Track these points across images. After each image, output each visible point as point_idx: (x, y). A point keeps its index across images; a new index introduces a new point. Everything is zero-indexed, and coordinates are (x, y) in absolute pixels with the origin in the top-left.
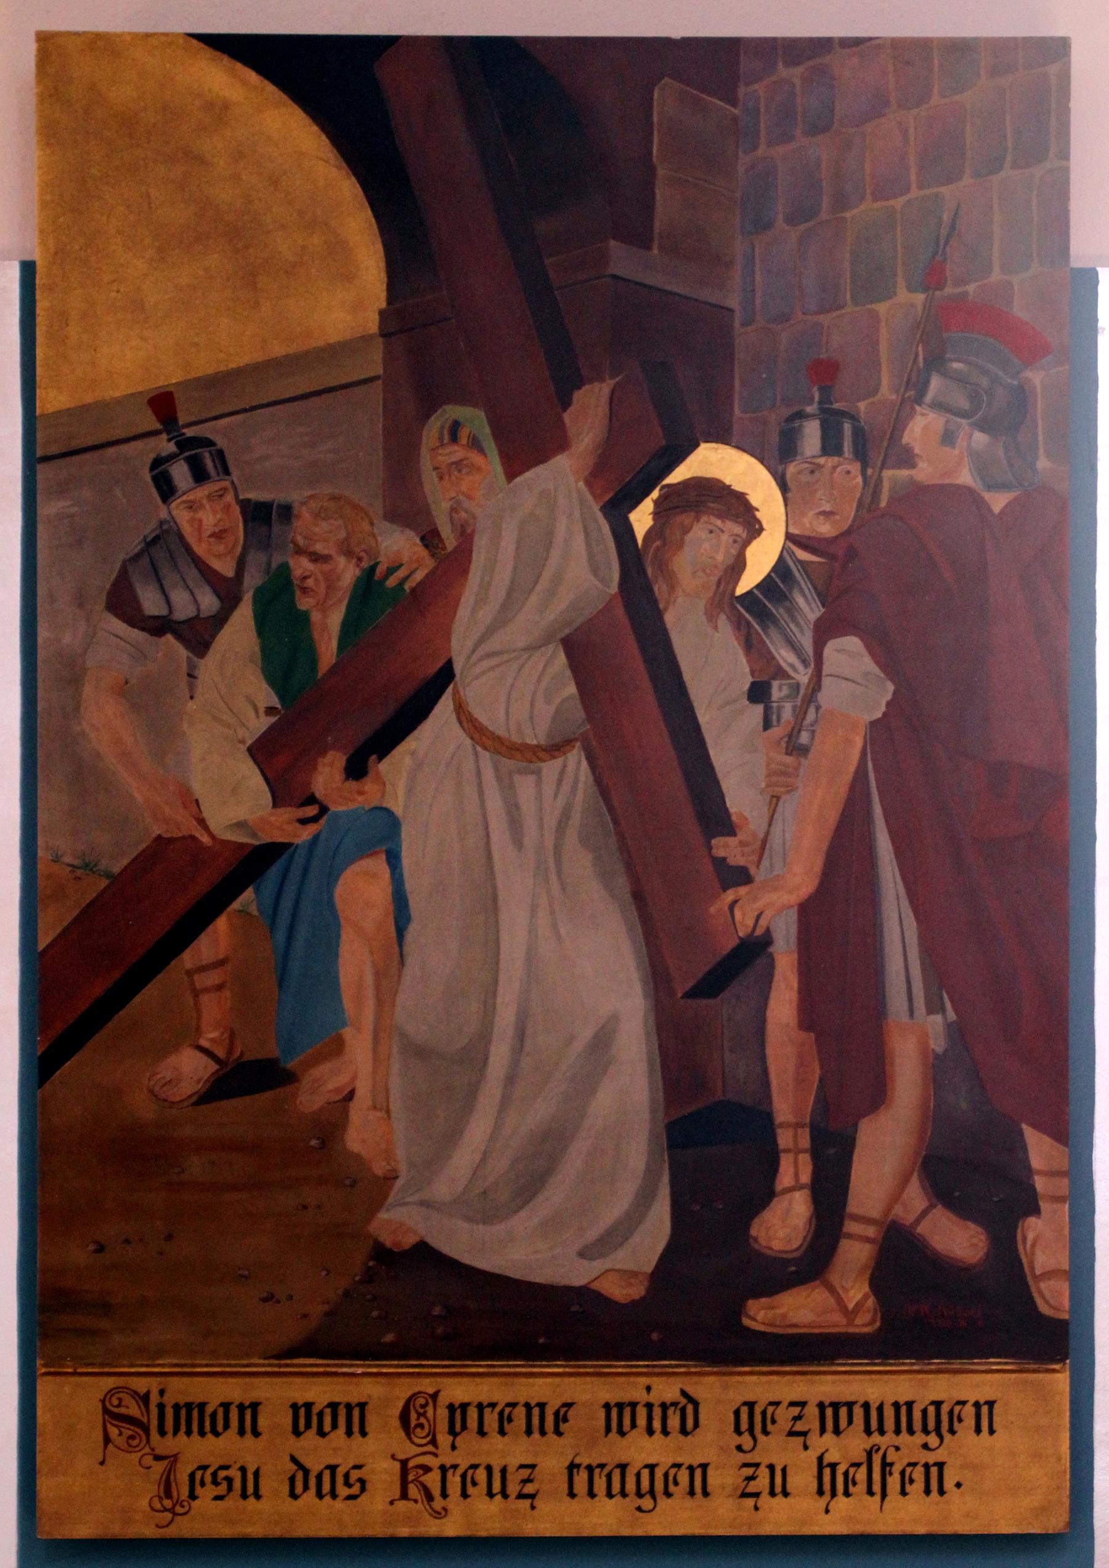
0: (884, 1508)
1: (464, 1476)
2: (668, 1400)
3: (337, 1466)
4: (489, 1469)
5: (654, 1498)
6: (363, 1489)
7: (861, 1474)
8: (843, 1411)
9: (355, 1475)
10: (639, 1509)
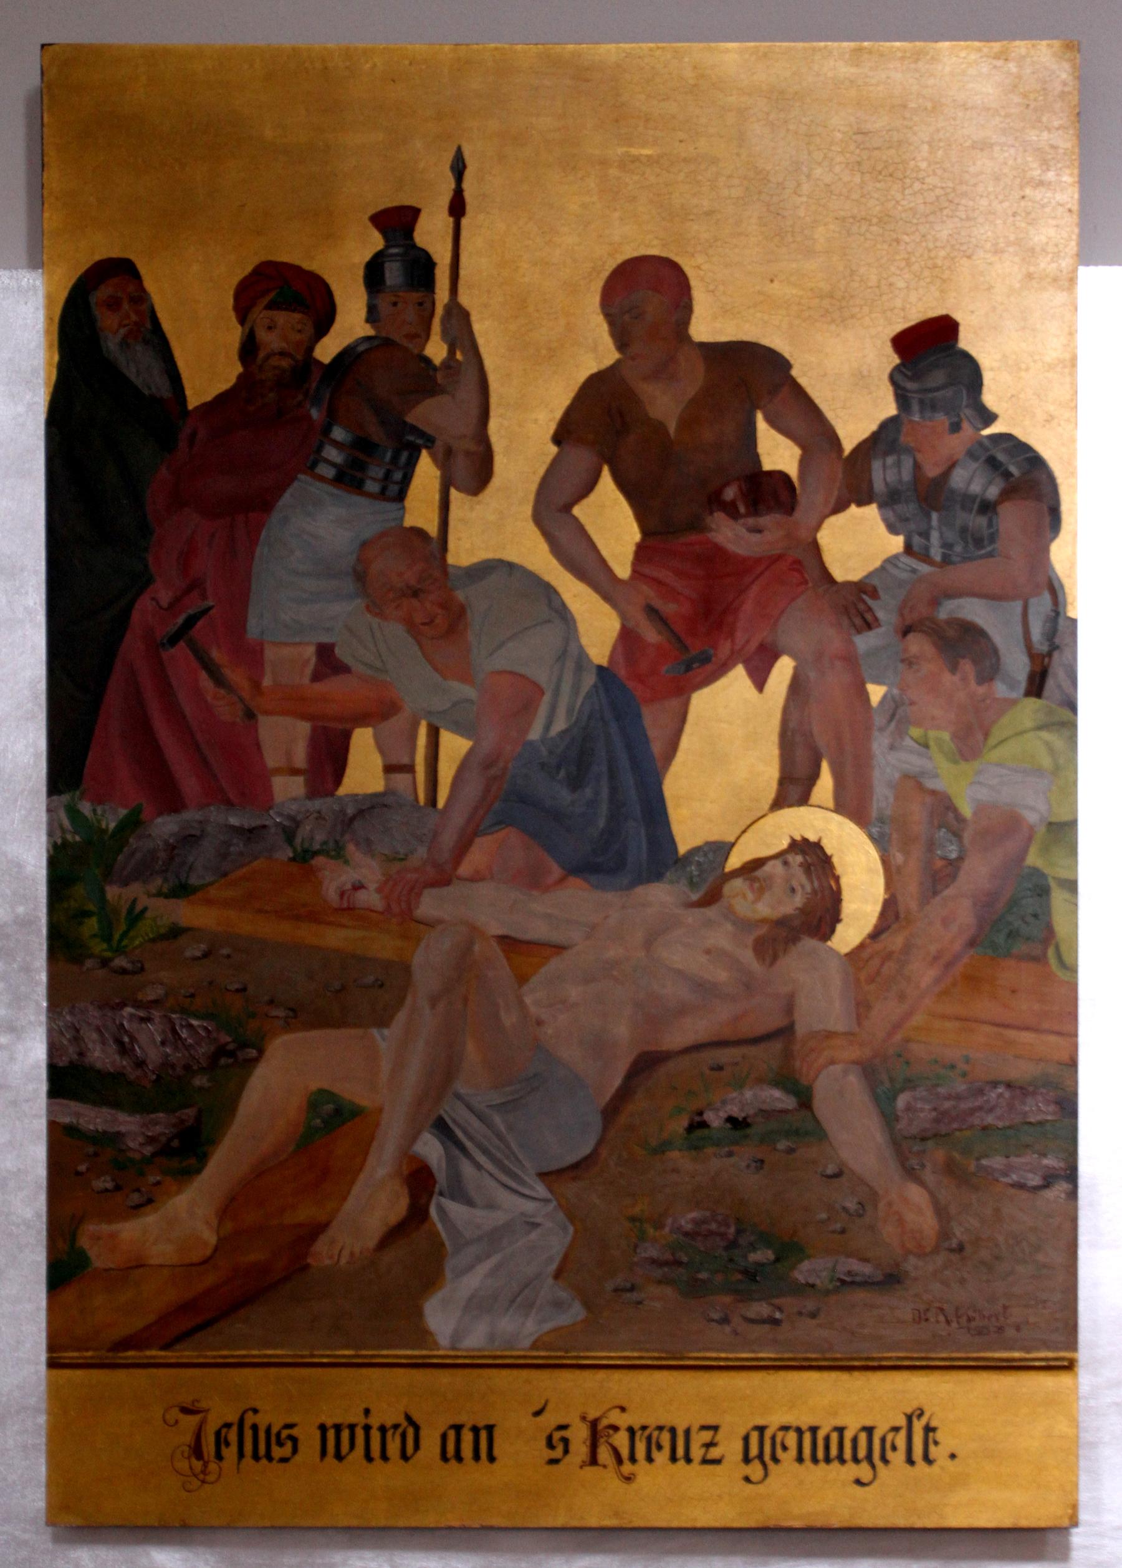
1: (649, 1439)
2: (389, 1423)
4: (673, 1431)
5: (873, 1466)
6: (295, 1450)
7: (901, 1440)
8: (345, 1435)
9: (557, 1436)
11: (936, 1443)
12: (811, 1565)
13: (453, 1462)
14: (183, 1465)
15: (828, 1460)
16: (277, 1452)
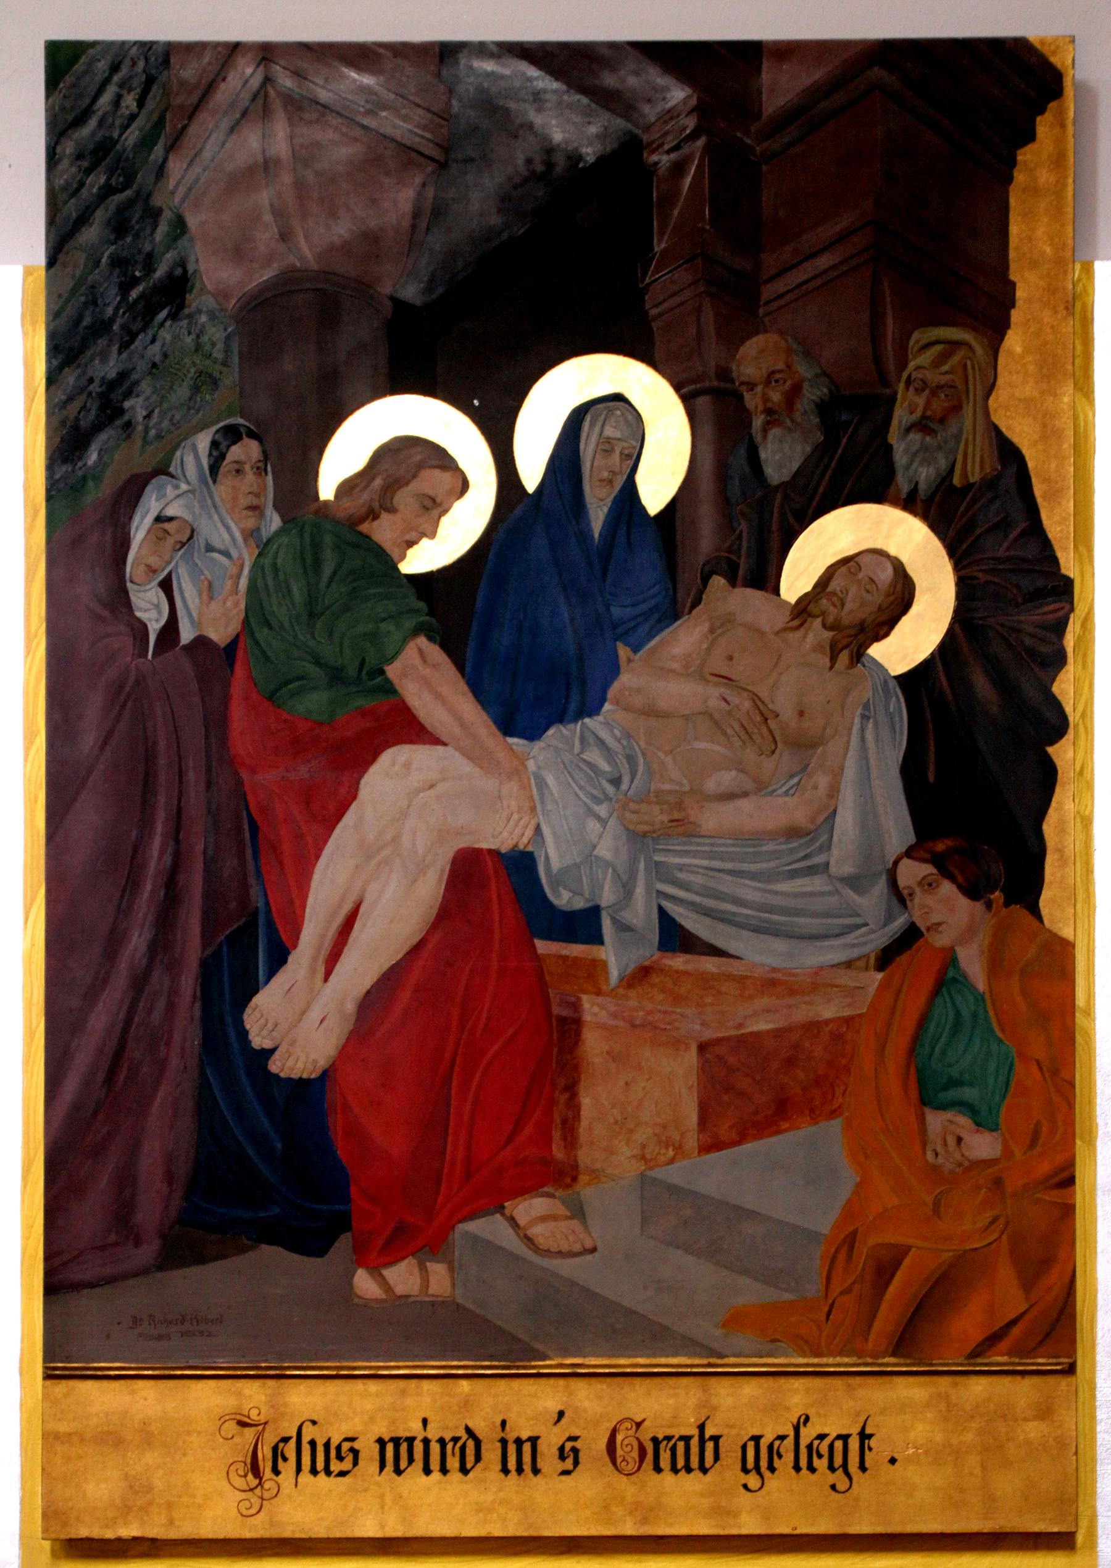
0: (300, 1480)
3: (760, 1437)
5: (759, 1473)
6: (576, 1463)
9: (346, 1446)
10: (745, 1486)
11: (870, 1449)
12: (578, 1562)
13: (683, 1473)
14: (240, 1483)
15: (689, 1469)
16: (336, 1467)
